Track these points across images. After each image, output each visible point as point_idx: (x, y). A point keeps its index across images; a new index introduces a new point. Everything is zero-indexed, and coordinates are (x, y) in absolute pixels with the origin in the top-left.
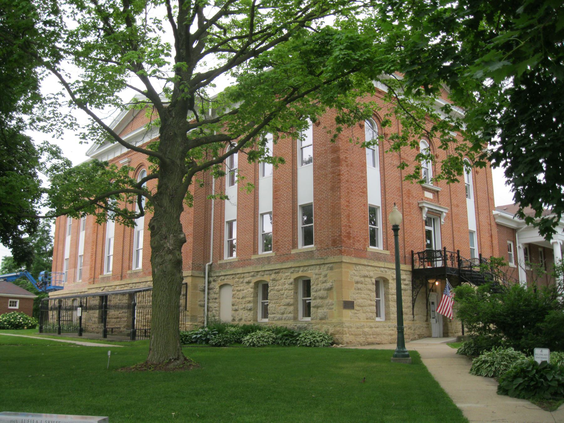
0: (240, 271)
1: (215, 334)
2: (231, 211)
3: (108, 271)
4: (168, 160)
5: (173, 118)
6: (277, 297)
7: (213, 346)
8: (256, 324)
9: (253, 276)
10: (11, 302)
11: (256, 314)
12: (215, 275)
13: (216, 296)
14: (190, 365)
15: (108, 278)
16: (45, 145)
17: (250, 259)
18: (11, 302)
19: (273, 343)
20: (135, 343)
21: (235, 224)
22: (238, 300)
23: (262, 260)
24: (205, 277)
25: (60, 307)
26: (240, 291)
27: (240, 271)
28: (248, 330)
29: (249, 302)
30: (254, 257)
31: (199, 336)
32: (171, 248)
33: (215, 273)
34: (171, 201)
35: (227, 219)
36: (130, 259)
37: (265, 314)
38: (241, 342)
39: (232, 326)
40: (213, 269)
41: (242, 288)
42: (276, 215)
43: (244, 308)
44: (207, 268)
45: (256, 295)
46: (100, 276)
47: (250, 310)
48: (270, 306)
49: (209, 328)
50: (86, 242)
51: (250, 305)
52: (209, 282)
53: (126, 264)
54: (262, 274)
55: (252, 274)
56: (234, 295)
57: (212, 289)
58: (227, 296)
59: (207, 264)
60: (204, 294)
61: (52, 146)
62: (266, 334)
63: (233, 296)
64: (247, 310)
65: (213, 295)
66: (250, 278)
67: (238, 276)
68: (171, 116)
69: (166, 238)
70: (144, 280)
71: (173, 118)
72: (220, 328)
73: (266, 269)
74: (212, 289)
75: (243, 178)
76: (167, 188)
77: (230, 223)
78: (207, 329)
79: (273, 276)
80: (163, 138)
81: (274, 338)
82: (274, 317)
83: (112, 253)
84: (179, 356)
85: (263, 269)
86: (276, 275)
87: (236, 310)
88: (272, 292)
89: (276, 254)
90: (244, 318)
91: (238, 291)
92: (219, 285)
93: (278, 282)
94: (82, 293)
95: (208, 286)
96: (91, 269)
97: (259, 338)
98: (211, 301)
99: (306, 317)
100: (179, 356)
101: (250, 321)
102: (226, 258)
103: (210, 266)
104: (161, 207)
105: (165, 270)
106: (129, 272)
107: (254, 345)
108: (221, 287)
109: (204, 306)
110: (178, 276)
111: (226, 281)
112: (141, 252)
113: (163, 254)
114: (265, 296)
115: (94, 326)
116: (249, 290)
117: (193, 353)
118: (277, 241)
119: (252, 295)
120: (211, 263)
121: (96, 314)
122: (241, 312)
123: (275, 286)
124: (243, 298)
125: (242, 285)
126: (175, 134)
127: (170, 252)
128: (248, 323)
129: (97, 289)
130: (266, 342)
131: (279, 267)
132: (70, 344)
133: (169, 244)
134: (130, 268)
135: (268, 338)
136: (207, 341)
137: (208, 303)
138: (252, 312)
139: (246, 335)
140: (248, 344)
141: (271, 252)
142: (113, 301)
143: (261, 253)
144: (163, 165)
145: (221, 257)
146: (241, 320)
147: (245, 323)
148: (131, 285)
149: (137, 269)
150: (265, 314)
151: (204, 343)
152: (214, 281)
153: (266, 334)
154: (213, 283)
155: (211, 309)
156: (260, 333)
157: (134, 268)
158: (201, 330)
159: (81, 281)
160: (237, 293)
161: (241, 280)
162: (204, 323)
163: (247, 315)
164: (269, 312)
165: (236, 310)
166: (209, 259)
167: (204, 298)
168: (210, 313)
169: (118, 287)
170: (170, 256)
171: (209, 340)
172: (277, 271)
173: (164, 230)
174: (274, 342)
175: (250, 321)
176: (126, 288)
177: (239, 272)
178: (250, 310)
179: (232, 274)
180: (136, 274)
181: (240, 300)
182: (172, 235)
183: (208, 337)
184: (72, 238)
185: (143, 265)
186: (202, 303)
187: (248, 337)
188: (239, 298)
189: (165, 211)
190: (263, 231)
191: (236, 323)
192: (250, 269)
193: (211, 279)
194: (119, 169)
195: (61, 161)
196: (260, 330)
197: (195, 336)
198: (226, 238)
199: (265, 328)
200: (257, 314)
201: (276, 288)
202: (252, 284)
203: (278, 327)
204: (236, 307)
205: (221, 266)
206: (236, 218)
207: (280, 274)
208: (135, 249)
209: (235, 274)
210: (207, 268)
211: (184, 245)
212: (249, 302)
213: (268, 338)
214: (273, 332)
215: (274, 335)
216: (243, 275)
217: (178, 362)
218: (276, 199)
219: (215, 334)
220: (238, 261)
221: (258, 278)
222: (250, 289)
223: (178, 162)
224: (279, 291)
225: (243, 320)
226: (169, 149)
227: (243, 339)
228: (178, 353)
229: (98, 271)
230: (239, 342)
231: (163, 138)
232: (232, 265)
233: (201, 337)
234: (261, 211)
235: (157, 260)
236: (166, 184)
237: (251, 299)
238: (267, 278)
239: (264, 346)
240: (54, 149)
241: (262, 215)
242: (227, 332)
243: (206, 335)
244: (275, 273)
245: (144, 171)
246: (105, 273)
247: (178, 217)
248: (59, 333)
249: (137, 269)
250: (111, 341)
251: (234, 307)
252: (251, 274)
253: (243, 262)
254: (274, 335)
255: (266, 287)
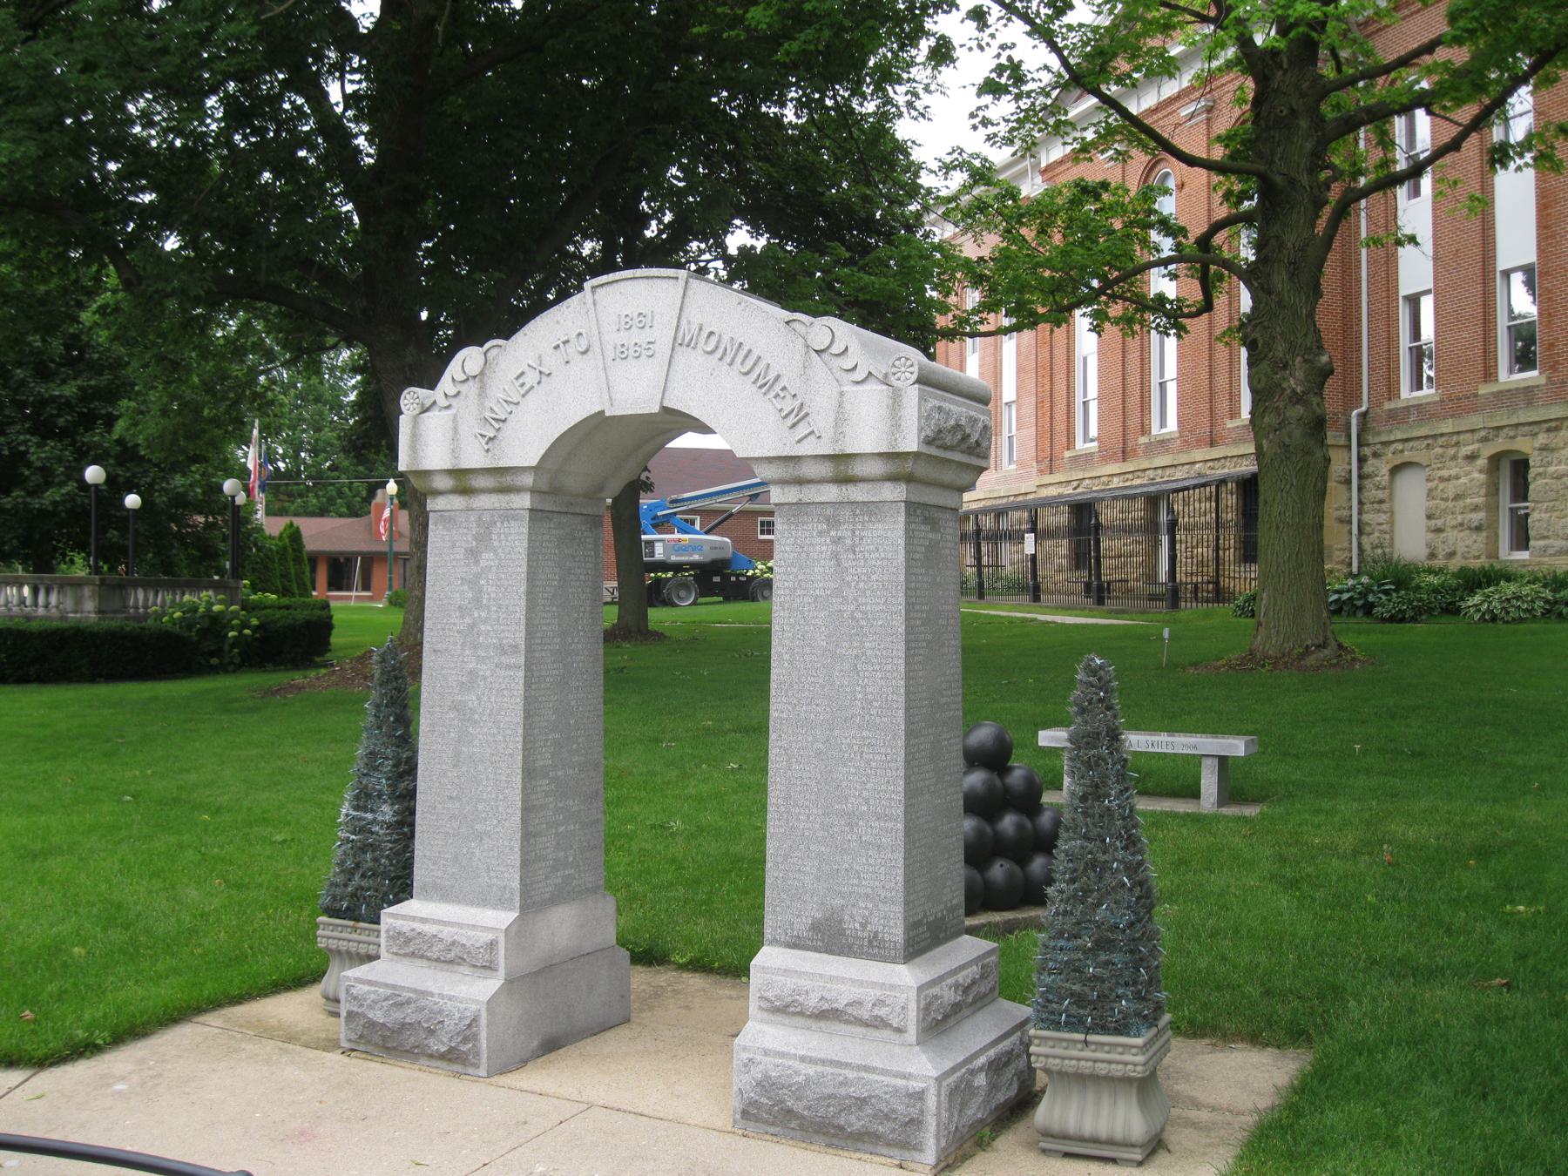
0: (1447, 427)
1: (1386, 592)
2: (1415, 270)
3: (1086, 439)
4: (1278, 179)
5: (1286, 71)
6: (1553, 495)
7: (1383, 620)
8: (1497, 566)
9: (1485, 440)
10: (762, 523)
11: (1494, 539)
12: (1377, 440)
13: (1381, 495)
14: (1354, 659)
15: (1088, 457)
16: (956, 155)
17: (1476, 396)
18: (762, 523)
19: (1546, 613)
20: (1182, 615)
21: (1427, 306)
22: (1443, 505)
23: (1509, 397)
24: (1349, 447)
25: (978, 532)
26: (1448, 479)
27: (1447, 427)
28: (1474, 581)
29: (1476, 508)
30: (1484, 390)
31: (1345, 596)
32: (1299, 389)
33: (1378, 434)
34: (1292, 276)
35: (1405, 289)
36: (1145, 407)
37: (1521, 539)
38: (1458, 611)
39: (1430, 571)
40: (1371, 425)
41: (1453, 472)
42: (1547, 273)
43: (1461, 525)
44: (1354, 422)
45: (1493, 490)
46: (1067, 454)
47: (1478, 529)
48: (1534, 516)
49: (1371, 577)
50: (1020, 370)
51: (1478, 517)
52: (1362, 460)
53: (1134, 421)
54: (1512, 433)
55: (1483, 433)
56: (1430, 490)
57: (1368, 476)
58: (1412, 496)
59: (1355, 413)
60: (1350, 489)
61: (971, 155)
62: (1526, 590)
63: (1430, 494)
64: (1470, 528)
65: (1372, 494)
66: (1476, 446)
67: (1441, 441)
68: (1280, 66)
69: (1285, 366)
70: (1184, 458)
71: (1286, 71)
72: (1401, 577)
73: (1522, 420)
74: (1368, 476)
75: (1455, 183)
76: (1281, 246)
77: (1414, 301)
78: (1365, 579)
79: (1542, 439)
80: (1262, 123)
81: (1547, 601)
82: (1547, 547)
83: (1093, 392)
84: (1326, 638)
85: (1514, 421)
86: (1552, 435)
87: (1439, 530)
88: (1540, 482)
89: (1549, 378)
90: (1461, 550)
91: (1442, 479)
92: (1389, 466)
93: (1556, 455)
94: (1020, 498)
95: (1360, 468)
96: (1038, 437)
97: (1508, 600)
98: (1367, 507)
99: (1518, 549)
100: (1326, 638)
101: (1478, 557)
102: (1406, 393)
103: (1364, 415)
104: (1269, 293)
105: (1287, 441)
106: (1143, 440)
107: (1494, 619)
108: (1395, 470)
109: (1350, 522)
110: (1319, 454)
111: (1407, 456)
112: (1172, 390)
113: (1281, 404)
114: (1521, 490)
115: (1060, 577)
116: (1475, 476)
117: (1355, 635)
118: (1552, 345)
119: (1483, 491)
120: (1364, 409)
121: (1063, 548)
122: (1451, 535)
123: (1550, 464)
124: (1457, 498)
125: (1453, 464)
126: (1293, 112)
127: (1297, 399)
128: (1476, 564)
129: (1059, 485)
130: (1526, 611)
131: (1559, 415)
132: (1024, 620)
133: (1294, 381)
134: (1145, 429)
135: (1533, 601)
136: (1368, 609)
137: (1360, 513)
138: (1484, 534)
139: (1472, 592)
140: (1477, 617)
141: (1535, 373)
142: (1108, 514)
143: (1508, 377)
144: (1269, 192)
145: (1392, 390)
146: (1452, 554)
147: (1463, 563)
148: (1151, 473)
149: (1164, 431)
150: (1521, 539)
151: (1360, 614)
152: (1376, 455)
153: (1526, 590)
154: (1371, 461)
155: (1368, 529)
156: (1510, 589)
157: (1155, 430)
158: (1351, 582)
159: (1013, 467)
160: (1441, 486)
161: (1452, 451)
162: (1350, 564)
163: (1469, 542)
164: (1532, 533)
165: (1439, 530)
166: (1359, 397)
167: (1350, 499)
168: (1365, 539)
169: (1116, 479)
170: (1299, 410)
171: (1372, 605)
172: (1553, 424)
173: (1280, 348)
174: (1549, 611)
175: (1478, 557)
176: (1137, 482)
177: (1445, 430)
178: (1478, 529)
179: (1426, 437)
180: (1163, 444)
181: (1450, 504)
182: (1299, 359)
183: (1371, 598)
184: (982, 359)
185: (1180, 422)
186: (1345, 513)
187: (1477, 599)
188: (1446, 500)
189: (1279, 303)
190: (1511, 311)
191: (1438, 563)
192: (1475, 421)
193: (1367, 451)
194: (1132, 194)
195: (994, 191)
196: (1508, 580)
197: (1335, 597)
198: (1405, 342)
199: (1522, 577)
200: (1497, 540)
201: (1552, 469)
202: (1482, 462)
203: (1559, 572)
204: (1439, 523)
205: (1393, 415)
206: (1431, 286)
207: (1563, 432)
208: (1155, 380)
209: (1434, 437)
210: (1354, 422)
211: (1330, 380)
212: (1476, 508)
213: (1533, 601)
214: (1545, 586)
215: (1548, 594)
216: (1455, 438)
217: (1326, 652)
218: (1546, 227)
219: (1386, 592)
220: (1442, 401)
221: (1500, 445)
222: (1476, 475)
223: (1304, 179)
224: (1558, 478)
225: (1458, 557)
226: (1280, 150)
227: (1463, 605)
228: (1325, 631)
229: (1061, 439)
230: (1452, 610)
231: (1262, 123)
232: (1421, 411)
233: (1351, 598)
234: (1502, 263)
235: (1267, 420)
236: (1277, 237)
237: (1479, 500)
238: (1523, 445)
239: (1521, 620)
240: (977, 163)
241: (1507, 274)
242: (1418, 588)
243: (1364, 595)
244: (1549, 430)
245: (1167, 175)
246: (1080, 445)
247: (1311, 315)
248: (981, 596)
249: (1164, 431)
250: (1119, 613)
251: (1433, 522)
252: (1477, 436)
253: (1455, 405)
254: (1548, 594)
255: (1520, 467)
